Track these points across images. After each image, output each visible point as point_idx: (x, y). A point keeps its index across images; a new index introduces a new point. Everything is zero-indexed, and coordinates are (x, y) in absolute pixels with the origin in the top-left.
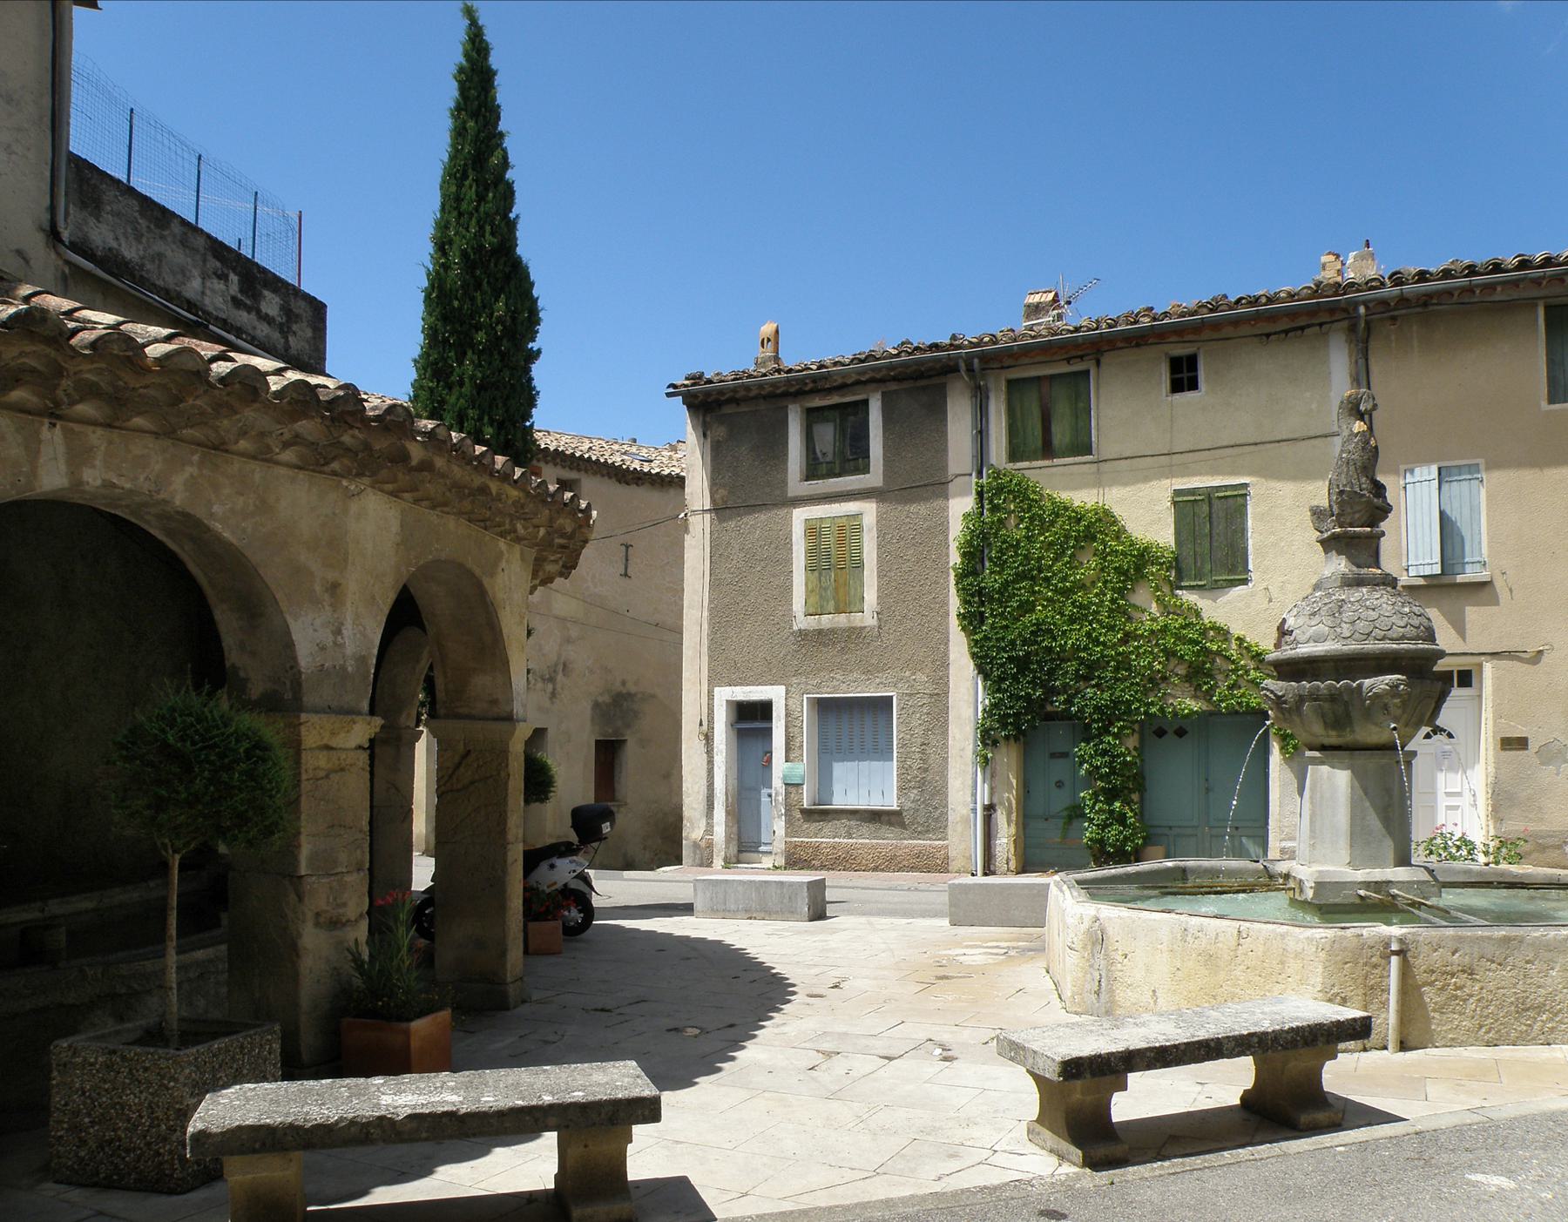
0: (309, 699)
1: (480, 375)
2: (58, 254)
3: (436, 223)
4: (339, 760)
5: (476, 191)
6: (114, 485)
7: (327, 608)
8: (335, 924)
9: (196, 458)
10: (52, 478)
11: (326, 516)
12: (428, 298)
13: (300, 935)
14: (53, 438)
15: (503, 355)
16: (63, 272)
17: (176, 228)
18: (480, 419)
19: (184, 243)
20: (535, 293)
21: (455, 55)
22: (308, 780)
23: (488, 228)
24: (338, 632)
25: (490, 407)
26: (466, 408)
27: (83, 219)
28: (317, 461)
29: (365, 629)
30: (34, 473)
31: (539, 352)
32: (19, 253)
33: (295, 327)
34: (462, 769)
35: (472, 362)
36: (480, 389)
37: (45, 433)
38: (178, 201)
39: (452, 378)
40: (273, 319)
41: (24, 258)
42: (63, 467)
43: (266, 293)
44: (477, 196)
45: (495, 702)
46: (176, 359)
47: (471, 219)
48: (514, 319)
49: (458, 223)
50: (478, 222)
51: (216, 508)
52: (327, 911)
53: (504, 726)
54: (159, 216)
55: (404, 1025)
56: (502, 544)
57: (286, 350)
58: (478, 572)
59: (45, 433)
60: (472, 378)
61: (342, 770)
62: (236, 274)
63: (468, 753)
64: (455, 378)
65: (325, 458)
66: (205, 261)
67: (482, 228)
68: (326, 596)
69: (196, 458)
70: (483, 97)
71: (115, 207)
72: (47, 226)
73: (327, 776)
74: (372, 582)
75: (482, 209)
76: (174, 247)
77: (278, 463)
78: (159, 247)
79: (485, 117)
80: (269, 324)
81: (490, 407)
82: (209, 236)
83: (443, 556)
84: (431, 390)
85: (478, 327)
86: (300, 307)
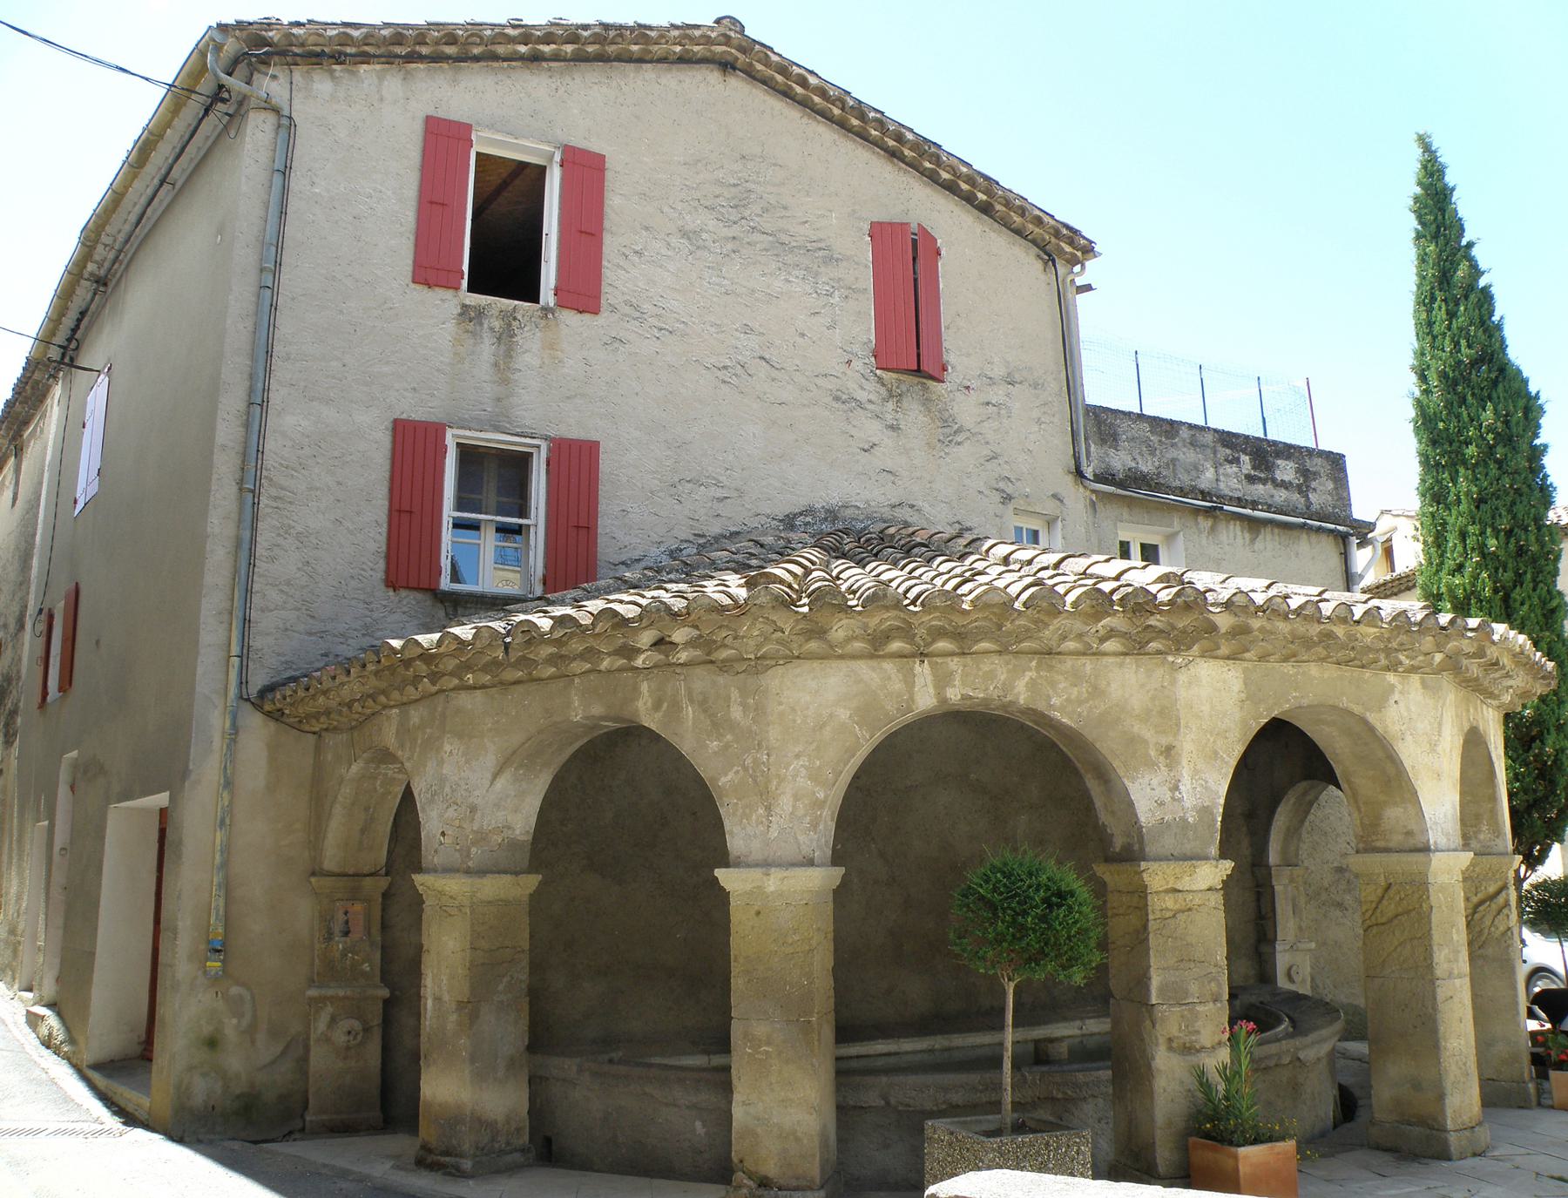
0: (1150, 849)
1: (1475, 489)
2: (1085, 487)
3: (1415, 353)
4: (1185, 900)
5: (1447, 310)
6: (971, 698)
7: (1163, 768)
8: (1188, 1050)
9: (1034, 663)
10: (925, 700)
11: (1156, 689)
12: (1417, 430)
13: (1153, 1058)
14: (923, 671)
15: (1499, 463)
16: (1091, 500)
17: (1185, 433)
18: (1483, 533)
19: (1193, 444)
20: (1533, 389)
21: (1408, 187)
22: (1155, 920)
23: (1463, 342)
24: (1176, 788)
25: (1493, 518)
26: (1466, 526)
27: (1105, 453)
28: (1136, 647)
29: (1207, 782)
30: (912, 698)
31: (1546, 446)
32: (1055, 496)
33: (1314, 484)
34: (1385, 902)
35: (1466, 478)
36: (1480, 502)
37: (917, 668)
38: (1185, 411)
39: (1450, 499)
40: (1290, 483)
41: (1059, 499)
42: (932, 690)
43: (1279, 462)
44: (1447, 314)
45: (1409, 833)
46: (984, 598)
47: (1444, 338)
48: (1507, 423)
49: (1432, 347)
50: (1452, 340)
51: (1053, 701)
52: (1178, 1038)
53: (1418, 857)
54: (1167, 428)
55: (1233, 1149)
56: (1391, 677)
57: (1308, 508)
58: (1357, 709)
59: (917, 668)
60: (1468, 493)
61: (1190, 909)
62: (1246, 454)
63: (1389, 886)
64: (1452, 498)
65: (1140, 643)
66: (1215, 453)
67: (1457, 344)
68: (1162, 759)
69: (1034, 663)
70: (1440, 217)
71: (1129, 434)
72: (1073, 468)
73: (1174, 916)
74: (1212, 740)
75: (1454, 325)
76: (1184, 450)
77: (1105, 654)
78: (1172, 453)
79: (1445, 236)
80: (1286, 488)
81: (1493, 518)
82: (1216, 431)
83: (1305, 702)
84: (1433, 515)
85: (1467, 443)
86: (1316, 464)
